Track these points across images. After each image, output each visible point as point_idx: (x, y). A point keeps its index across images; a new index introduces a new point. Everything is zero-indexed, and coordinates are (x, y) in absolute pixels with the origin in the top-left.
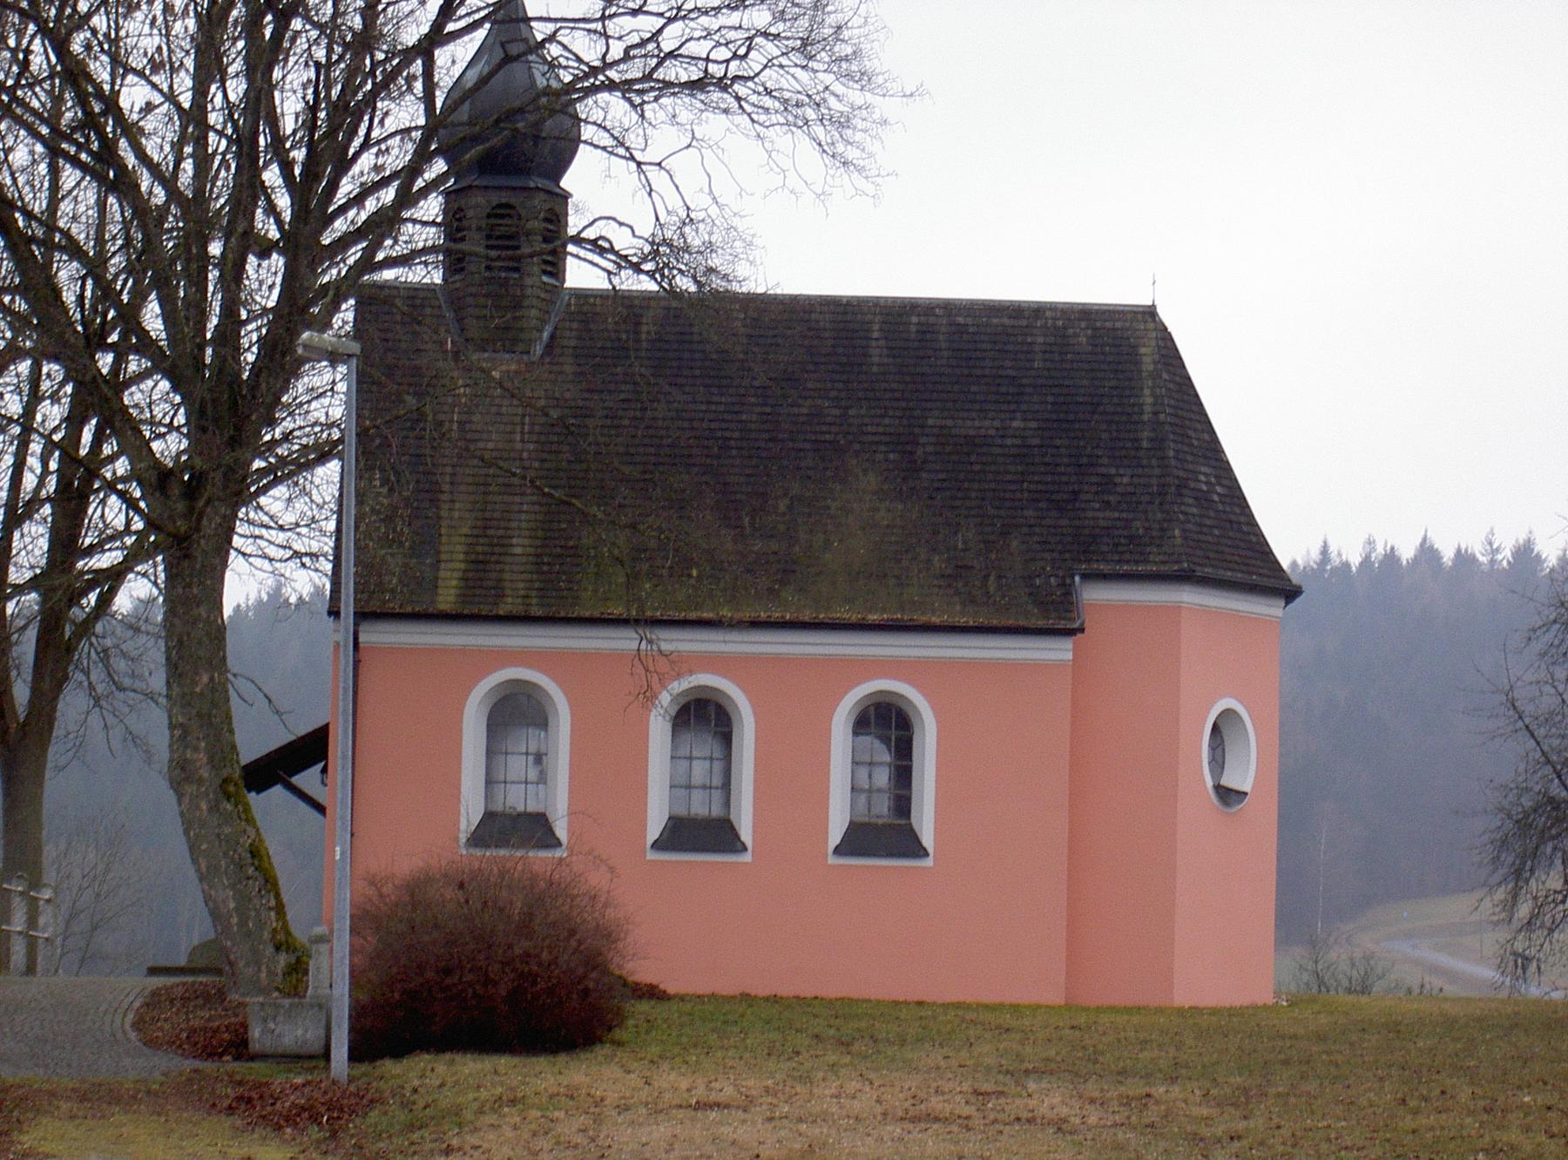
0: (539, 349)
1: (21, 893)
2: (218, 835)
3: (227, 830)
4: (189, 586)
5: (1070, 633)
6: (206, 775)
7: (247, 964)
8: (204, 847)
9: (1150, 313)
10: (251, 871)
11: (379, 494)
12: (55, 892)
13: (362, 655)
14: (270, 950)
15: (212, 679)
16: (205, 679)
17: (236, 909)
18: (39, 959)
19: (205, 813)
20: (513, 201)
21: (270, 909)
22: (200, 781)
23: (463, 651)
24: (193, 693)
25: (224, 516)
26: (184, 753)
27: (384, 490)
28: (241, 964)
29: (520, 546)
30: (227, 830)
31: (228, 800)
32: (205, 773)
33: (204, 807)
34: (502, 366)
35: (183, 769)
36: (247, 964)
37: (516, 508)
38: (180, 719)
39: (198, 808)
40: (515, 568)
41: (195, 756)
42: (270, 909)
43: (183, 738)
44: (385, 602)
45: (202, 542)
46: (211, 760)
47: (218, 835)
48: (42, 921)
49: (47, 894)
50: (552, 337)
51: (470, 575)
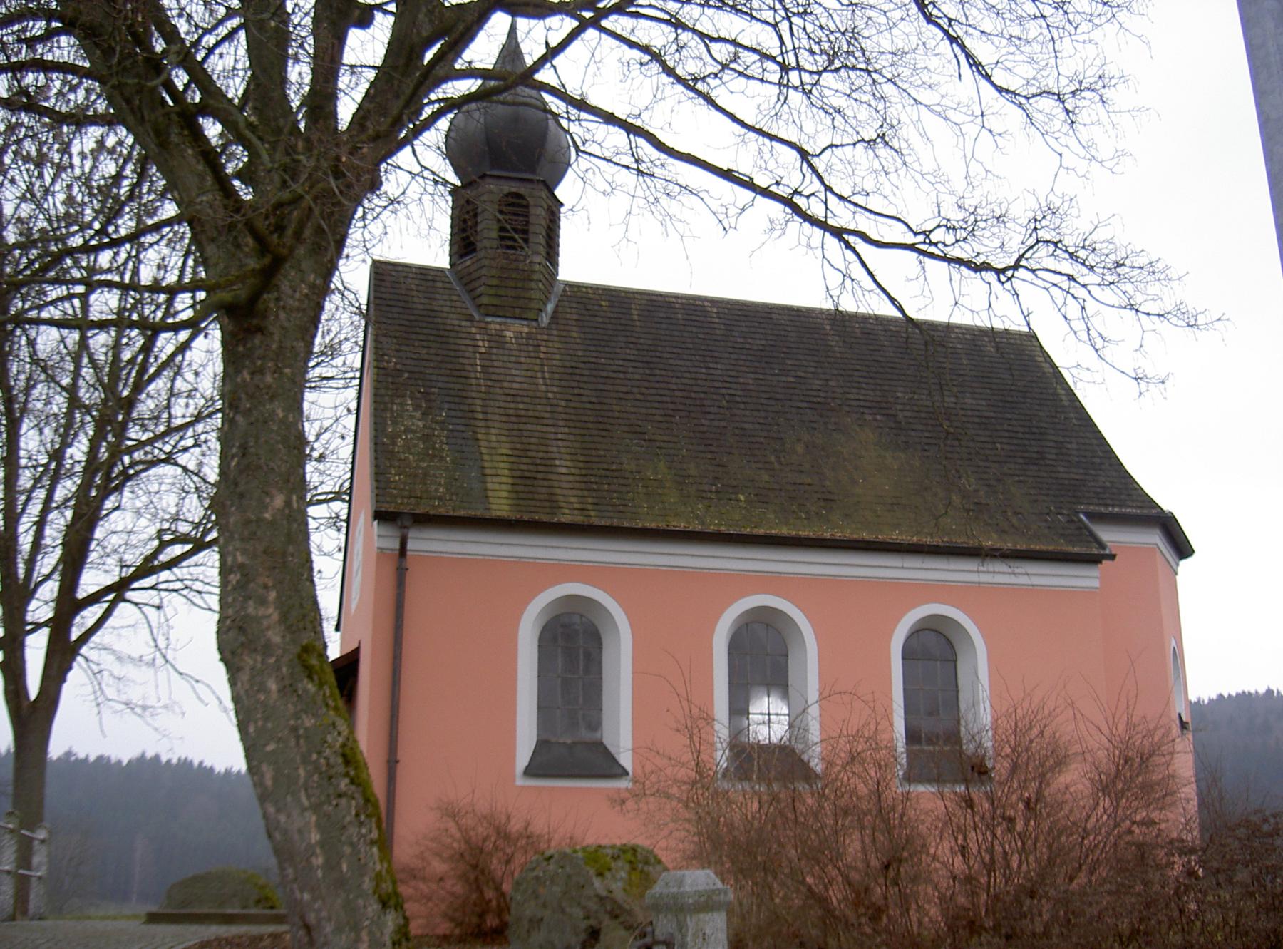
0: (545, 319)
1: (12, 831)
2: (294, 729)
3: (309, 722)
4: (261, 371)
5: (1094, 560)
6: (277, 639)
7: (339, 930)
8: (270, 748)
9: (1032, 337)
10: (343, 784)
11: (413, 417)
12: (50, 832)
13: (409, 563)
14: (373, 907)
15: (288, 503)
16: (279, 501)
17: (322, 844)
18: (32, 896)
19: (275, 696)
20: (522, 191)
21: (373, 843)
22: (267, 649)
23: (519, 562)
24: (259, 521)
25: (313, 286)
26: (243, 608)
27: (418, 414)
28: (329, 928)
29: (563, 466)
30: (309, 722)
31: (310, 677)
32: (275, 637)
33: (273, 686)
34: (512, 330)
35: (241, 629)
36: (339, 930)
37: (552, 436)
38: (240, 559)
39: (263, 689)
40: (565, 485)
41: (262, 611)
42: (373, 843)
43: (241, 586)
44: (434, 507)
45: (282, 315)
46: (284, 617)
47: (294, 729)
48: (36, 860)
49: (41, 834)
50: (555, 312)
51: (520, 488)
